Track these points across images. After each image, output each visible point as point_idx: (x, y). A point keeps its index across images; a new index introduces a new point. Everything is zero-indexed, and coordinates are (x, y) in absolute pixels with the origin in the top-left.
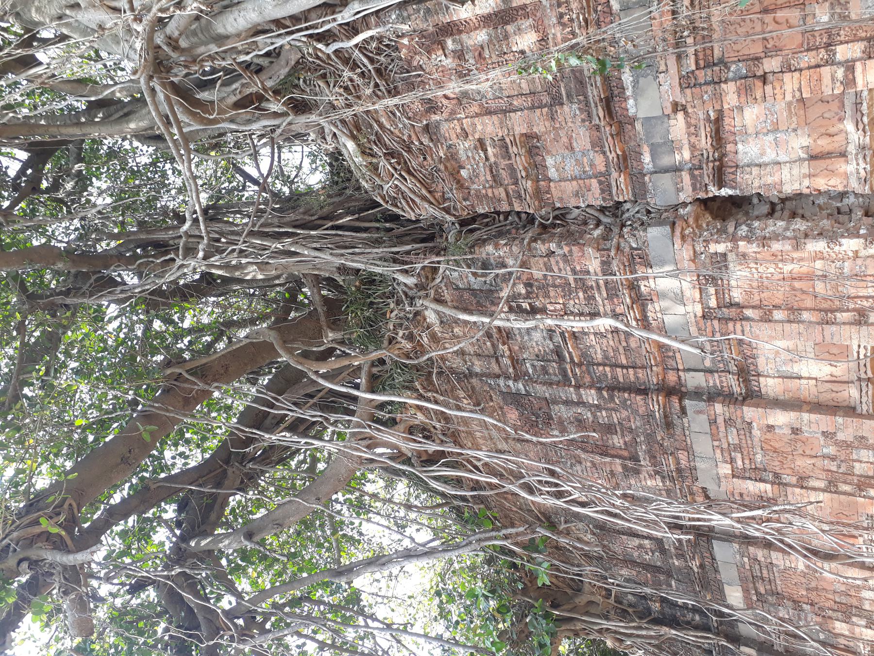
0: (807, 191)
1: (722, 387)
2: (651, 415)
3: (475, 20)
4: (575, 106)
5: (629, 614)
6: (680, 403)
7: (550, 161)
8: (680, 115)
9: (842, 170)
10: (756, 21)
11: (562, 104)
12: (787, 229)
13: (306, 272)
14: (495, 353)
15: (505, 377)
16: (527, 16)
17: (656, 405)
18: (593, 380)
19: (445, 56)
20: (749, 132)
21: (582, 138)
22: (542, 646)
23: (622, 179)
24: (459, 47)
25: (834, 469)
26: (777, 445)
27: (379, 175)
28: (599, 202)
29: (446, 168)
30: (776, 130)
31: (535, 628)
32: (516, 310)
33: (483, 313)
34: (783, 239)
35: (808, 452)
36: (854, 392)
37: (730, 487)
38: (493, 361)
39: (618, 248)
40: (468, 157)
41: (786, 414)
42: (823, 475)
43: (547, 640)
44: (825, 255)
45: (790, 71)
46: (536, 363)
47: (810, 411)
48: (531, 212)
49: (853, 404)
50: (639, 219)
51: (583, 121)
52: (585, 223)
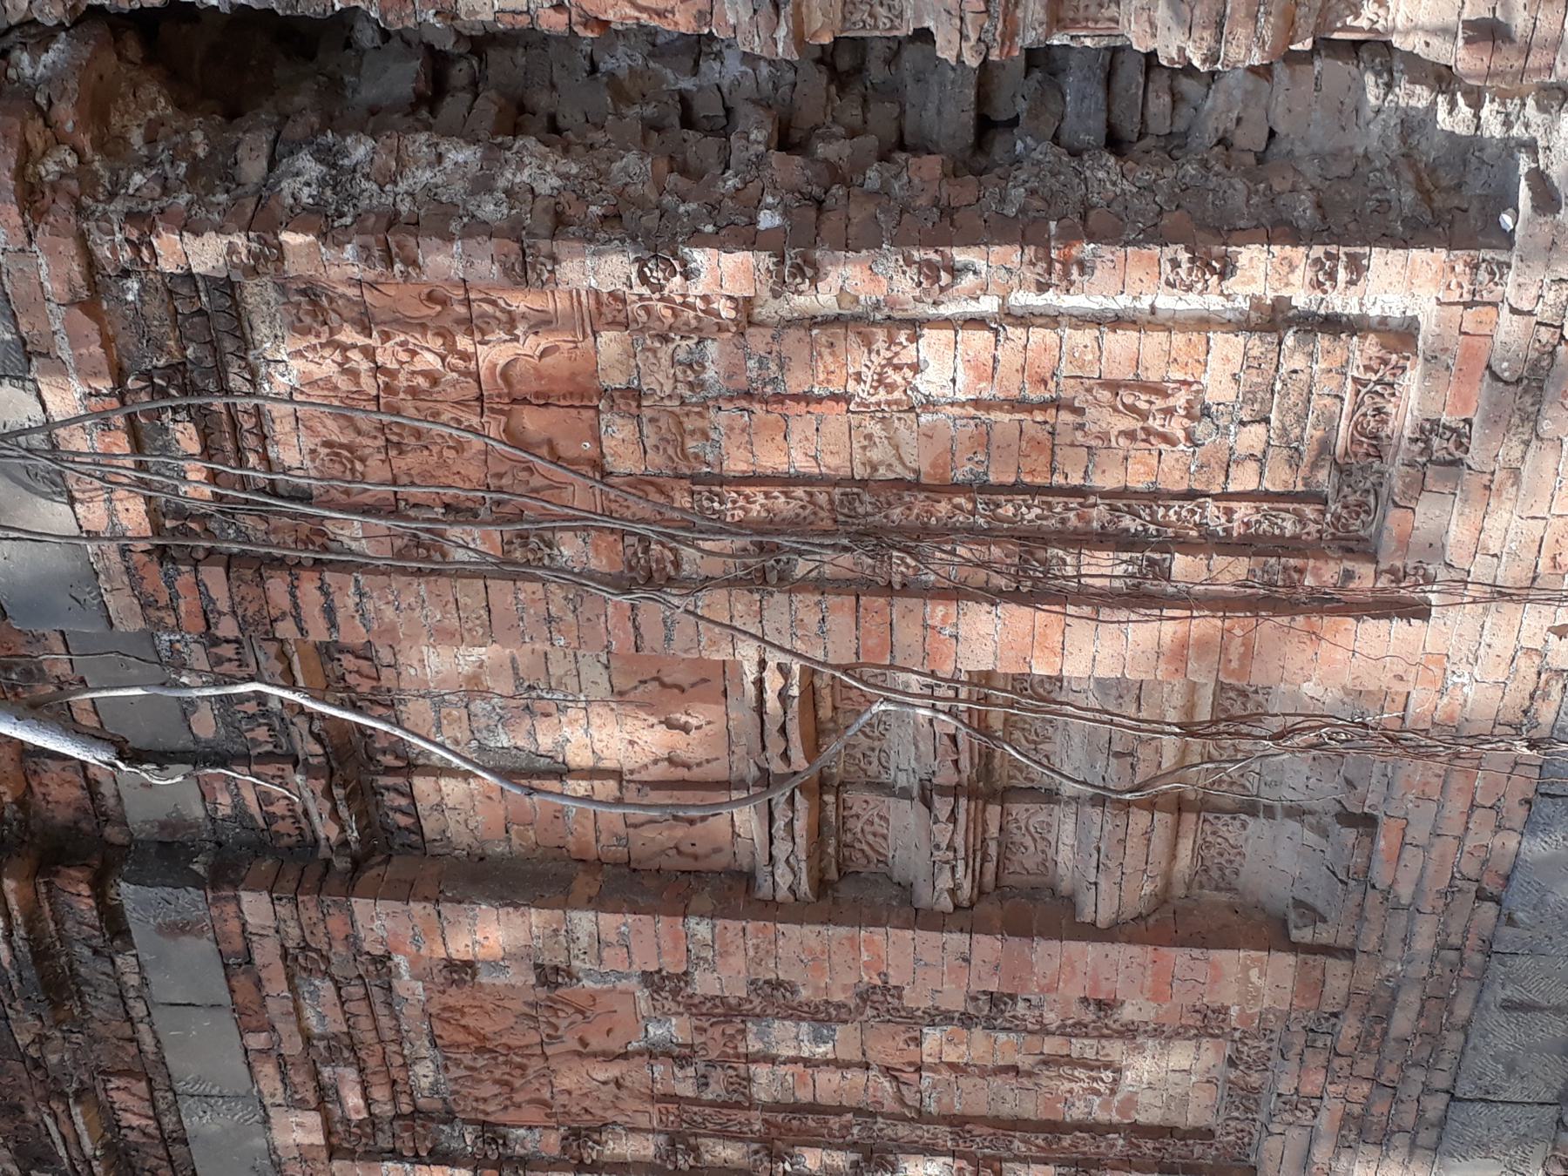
1: (270, 818)
12: (482, 185)
25: (687, 1089)
26: (487, 1026)
34: (467, 233)
35: (596, 1043)
36: (748, 820)
41: (514, 916)
42: (650, 1115)
47: (598, 903)
49: (744, 862)
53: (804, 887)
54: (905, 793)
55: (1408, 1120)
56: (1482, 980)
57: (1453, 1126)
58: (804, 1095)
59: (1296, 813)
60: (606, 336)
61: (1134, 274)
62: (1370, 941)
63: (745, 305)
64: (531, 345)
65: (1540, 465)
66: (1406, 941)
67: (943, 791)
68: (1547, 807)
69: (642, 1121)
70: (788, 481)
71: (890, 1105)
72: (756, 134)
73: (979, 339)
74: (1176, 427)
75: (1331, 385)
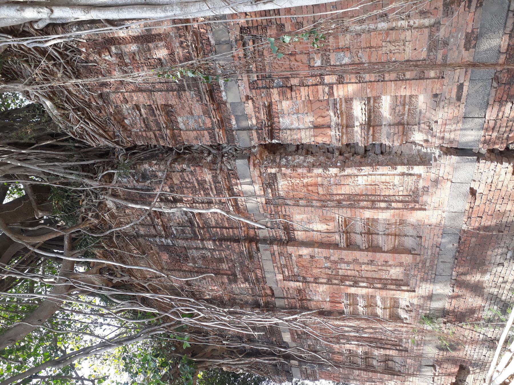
0: (313, 143)
1: (277, 236)
2: (242, 252)
3: (129, 38)
4: (192, 93)
5: (235, 353)
6: (256, 246)
7: (180, 119)
8: (250, 102)
9: (328, 134)
10: (286, 59)
11: (185, 90)
12: (304, 161)
13: (20, 173)
14: (153, 223)
15: (160, 237)
16: (161, 40)
17: (244, 248)
18: (211, 236)
19: (111, 56)
20: (285, 113)
21: (198, 109)
22: (187, 379)
23: (221, 132)
24: (120, 52)
25: (330, 273)
26: (304, 263)
27: (70, 121)
28: (209, 143)
29: (115, 119)
30: (298, 113)
31: (183, 371)
32: (164, 200)
33: (144, 203)
34: (303, 167)
35: (318, 266)
36: (337, 237)
37: (283, 286)
38: (152, 228)
39: (221, 169)
40: (129, 113)
41: (307, 249)
42: (325, 276)
43: (190, 377)
44: (322, 175)
45: (304, 86)
46: (178, 228)
47: (318, 247)
48: (171, 146)
49: (337, 243)
50: (231, 153)
51: (198, 101)
52: (202, 152)
53: (345, 246)
54: (358, 234)
55: (430, 278)
56: (438, 258)
57: (436, 279)
58: (346, 274)
59: (412, 236)
60: (319, 178)
61: (384, 169)
62: (422, 253)
63: (336, 175)
64: (310, 179)
65: (438, 192)
66: (427, 253)
67: (363, 233)
68: (444, 235)
69: (324, 277)
70: (342, 194)
71: (358, 276)
72: (337, 154)
73: (365, 177)
74: (391, 187)
75: (411, 182)
